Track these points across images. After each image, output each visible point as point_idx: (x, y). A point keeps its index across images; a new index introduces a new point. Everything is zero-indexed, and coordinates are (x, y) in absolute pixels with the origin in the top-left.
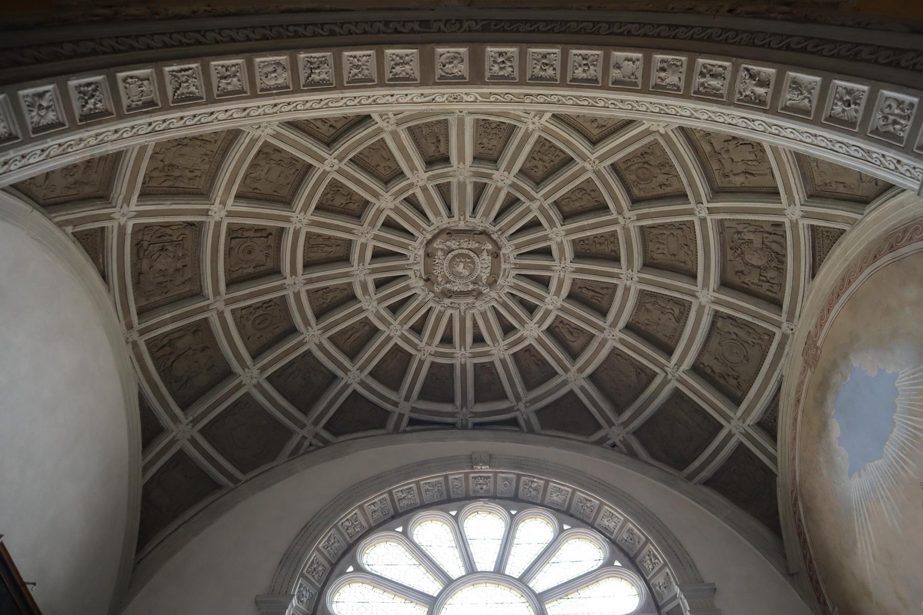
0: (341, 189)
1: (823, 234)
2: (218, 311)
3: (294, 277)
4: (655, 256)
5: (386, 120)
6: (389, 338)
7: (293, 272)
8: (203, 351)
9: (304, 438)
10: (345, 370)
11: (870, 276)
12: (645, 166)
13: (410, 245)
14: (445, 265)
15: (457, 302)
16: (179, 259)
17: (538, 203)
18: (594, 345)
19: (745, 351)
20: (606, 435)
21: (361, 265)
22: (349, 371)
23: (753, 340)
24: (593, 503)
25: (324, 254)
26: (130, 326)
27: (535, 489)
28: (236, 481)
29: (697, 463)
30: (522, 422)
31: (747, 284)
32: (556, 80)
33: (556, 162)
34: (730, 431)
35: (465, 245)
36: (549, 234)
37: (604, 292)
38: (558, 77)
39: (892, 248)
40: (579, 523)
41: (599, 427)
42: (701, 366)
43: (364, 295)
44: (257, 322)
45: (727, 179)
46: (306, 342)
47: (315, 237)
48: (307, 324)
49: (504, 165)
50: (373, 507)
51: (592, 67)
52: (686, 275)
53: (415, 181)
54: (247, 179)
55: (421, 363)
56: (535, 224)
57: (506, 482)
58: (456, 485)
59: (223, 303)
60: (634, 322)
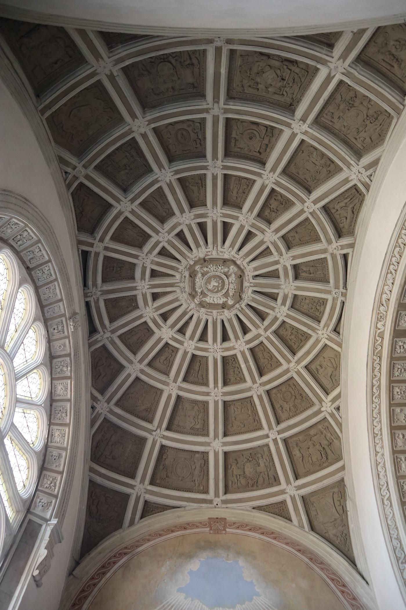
0: (283, 206)
1: (280, 507)
2: (210, 109)
3: (221, 167)
4: (232, 407)
5: (337, 248)
6: (157, 232)
7: (225, 167)
8: (173, 88)
9: (74, 168)
10: (133, 201)
11: (290, 552)
12: (294, 397)
13: (233, 249)
14: (216, 273)
15: (186, 281)
16: (266, 87)
17: (263, 333)
18: (163, 377)
19: (188, 475)
20: (99, 400)
21: (221, 215)
22: (132, 203)
23: (196, 480)
24: (65, 418)
25: (231, 188)
26: (229, 41)
27: (61, 370)
28: (43, 112)
29: (103, 471)
30: (96, 337)
31: (231, 468)
32: (392, 378)
33: (290, 343)
34: (135, 486)
35: (231, 286)
36: (240, 340)
37: (201, 378)
38: (395, 379)
39: (311, 559)
40: (49, 413)
41: (102, 392)
42: (166, 451)
43: (195, 215)
44: (184, 133)
45: (295, 446)
46: (161, 170)
47: (248, 184)
48: (177, 172)
49: (292, 313)
50: (37, 250)
51: (400, 396)
52: (225, 429)
53: (284, 257)
54: (314, 149)
55: (136, 257)
56: (245, 330)
57: (62, 347)
58: (55, 309)
59: (216, 114)
60: (182, 400)
